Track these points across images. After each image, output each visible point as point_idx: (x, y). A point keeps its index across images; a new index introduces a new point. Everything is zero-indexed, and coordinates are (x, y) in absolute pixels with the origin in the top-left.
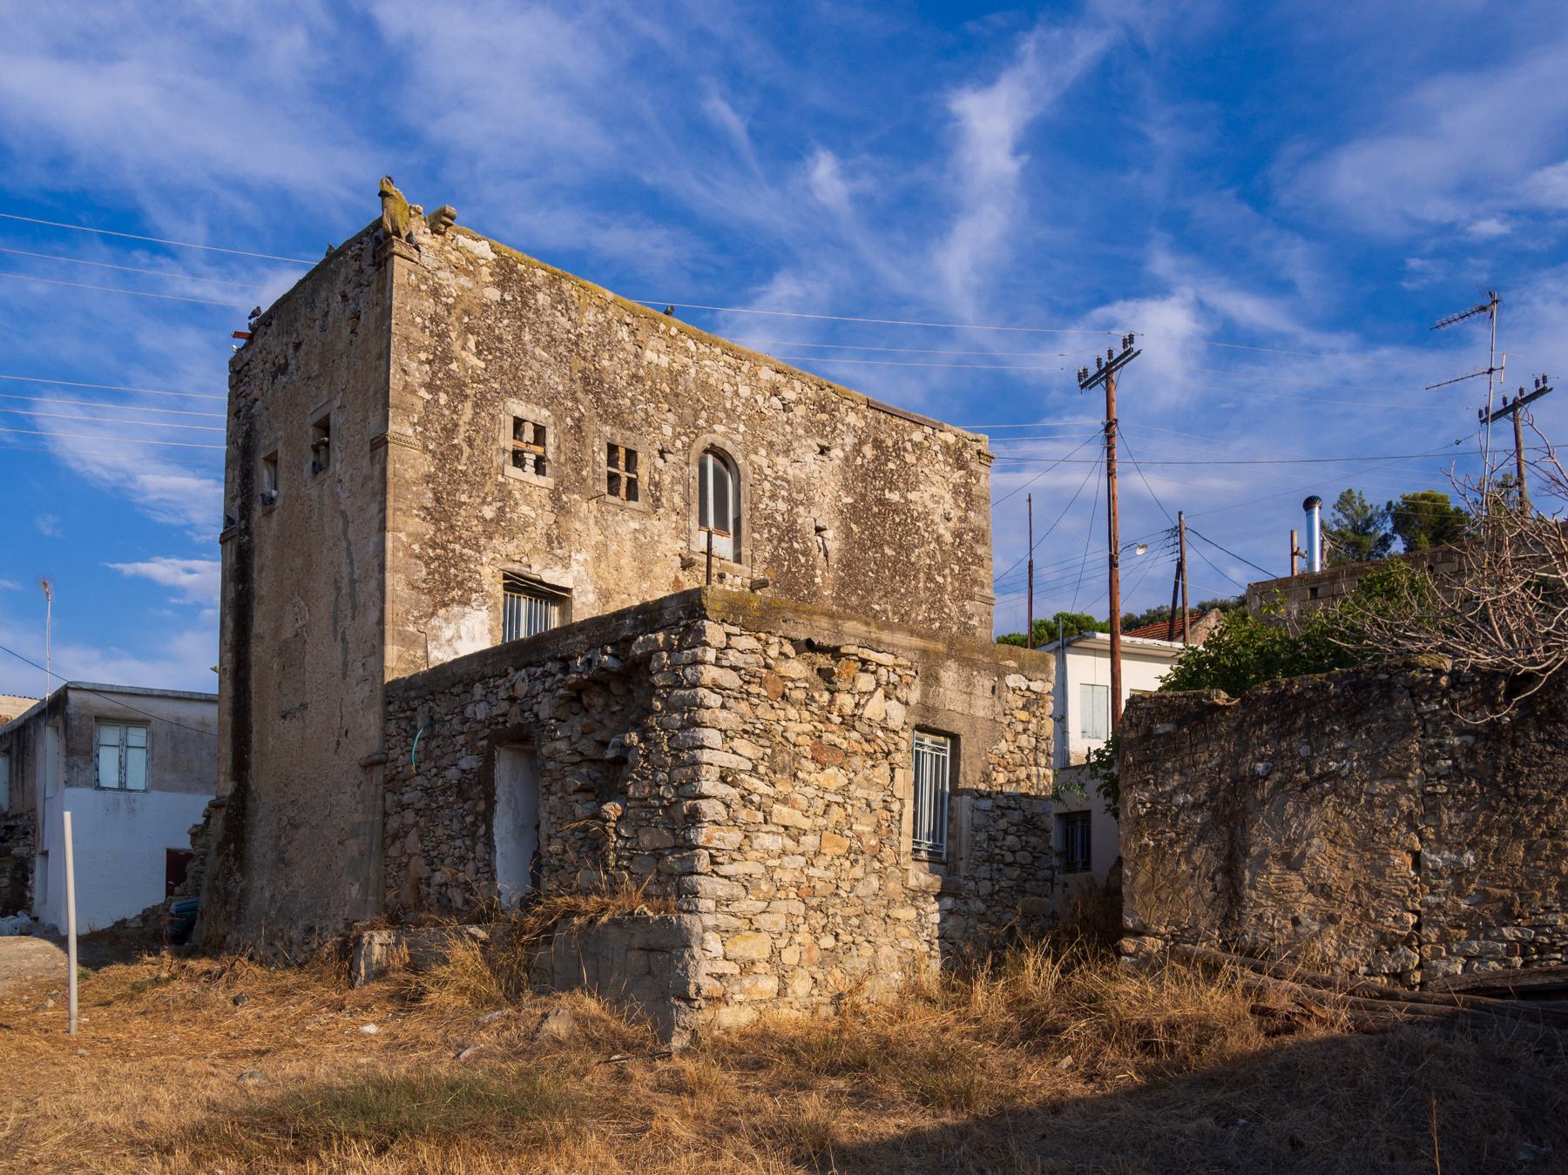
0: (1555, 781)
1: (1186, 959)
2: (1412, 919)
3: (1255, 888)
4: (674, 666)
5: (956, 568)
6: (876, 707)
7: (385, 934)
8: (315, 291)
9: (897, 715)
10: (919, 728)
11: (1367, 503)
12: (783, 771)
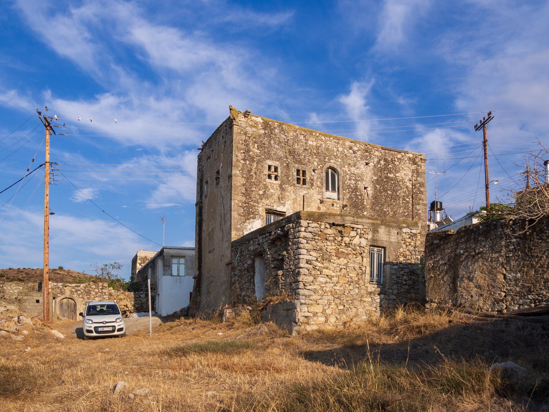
0: (542, 251)
2: (503, 294)
6: (356, 241)
8: (216, 136)
9: (364, 242)
10: (371, 246)
12: (326, 260)
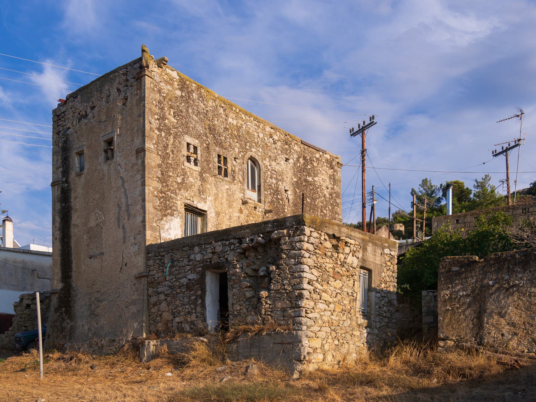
1: (462, 348)
3: (488, 324)
4: (291, 243)
5: (330, 207)
7: (155, 341)
11: (433, 184)
12: (325, 281)
